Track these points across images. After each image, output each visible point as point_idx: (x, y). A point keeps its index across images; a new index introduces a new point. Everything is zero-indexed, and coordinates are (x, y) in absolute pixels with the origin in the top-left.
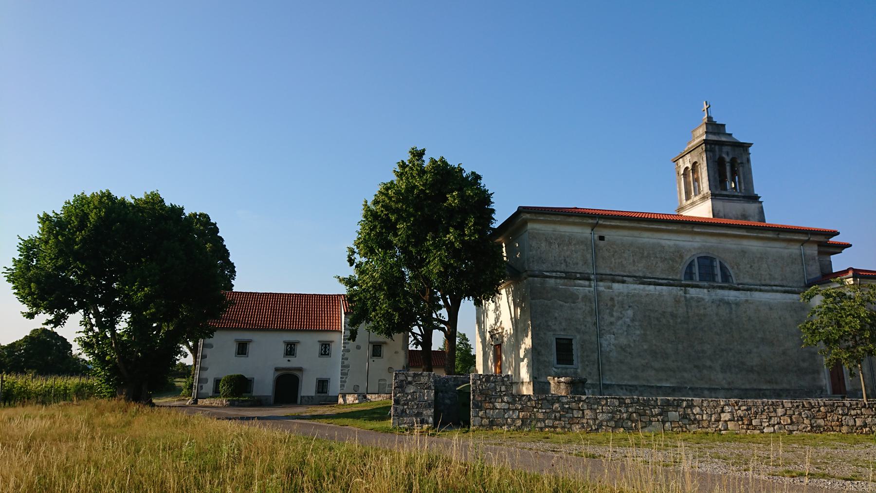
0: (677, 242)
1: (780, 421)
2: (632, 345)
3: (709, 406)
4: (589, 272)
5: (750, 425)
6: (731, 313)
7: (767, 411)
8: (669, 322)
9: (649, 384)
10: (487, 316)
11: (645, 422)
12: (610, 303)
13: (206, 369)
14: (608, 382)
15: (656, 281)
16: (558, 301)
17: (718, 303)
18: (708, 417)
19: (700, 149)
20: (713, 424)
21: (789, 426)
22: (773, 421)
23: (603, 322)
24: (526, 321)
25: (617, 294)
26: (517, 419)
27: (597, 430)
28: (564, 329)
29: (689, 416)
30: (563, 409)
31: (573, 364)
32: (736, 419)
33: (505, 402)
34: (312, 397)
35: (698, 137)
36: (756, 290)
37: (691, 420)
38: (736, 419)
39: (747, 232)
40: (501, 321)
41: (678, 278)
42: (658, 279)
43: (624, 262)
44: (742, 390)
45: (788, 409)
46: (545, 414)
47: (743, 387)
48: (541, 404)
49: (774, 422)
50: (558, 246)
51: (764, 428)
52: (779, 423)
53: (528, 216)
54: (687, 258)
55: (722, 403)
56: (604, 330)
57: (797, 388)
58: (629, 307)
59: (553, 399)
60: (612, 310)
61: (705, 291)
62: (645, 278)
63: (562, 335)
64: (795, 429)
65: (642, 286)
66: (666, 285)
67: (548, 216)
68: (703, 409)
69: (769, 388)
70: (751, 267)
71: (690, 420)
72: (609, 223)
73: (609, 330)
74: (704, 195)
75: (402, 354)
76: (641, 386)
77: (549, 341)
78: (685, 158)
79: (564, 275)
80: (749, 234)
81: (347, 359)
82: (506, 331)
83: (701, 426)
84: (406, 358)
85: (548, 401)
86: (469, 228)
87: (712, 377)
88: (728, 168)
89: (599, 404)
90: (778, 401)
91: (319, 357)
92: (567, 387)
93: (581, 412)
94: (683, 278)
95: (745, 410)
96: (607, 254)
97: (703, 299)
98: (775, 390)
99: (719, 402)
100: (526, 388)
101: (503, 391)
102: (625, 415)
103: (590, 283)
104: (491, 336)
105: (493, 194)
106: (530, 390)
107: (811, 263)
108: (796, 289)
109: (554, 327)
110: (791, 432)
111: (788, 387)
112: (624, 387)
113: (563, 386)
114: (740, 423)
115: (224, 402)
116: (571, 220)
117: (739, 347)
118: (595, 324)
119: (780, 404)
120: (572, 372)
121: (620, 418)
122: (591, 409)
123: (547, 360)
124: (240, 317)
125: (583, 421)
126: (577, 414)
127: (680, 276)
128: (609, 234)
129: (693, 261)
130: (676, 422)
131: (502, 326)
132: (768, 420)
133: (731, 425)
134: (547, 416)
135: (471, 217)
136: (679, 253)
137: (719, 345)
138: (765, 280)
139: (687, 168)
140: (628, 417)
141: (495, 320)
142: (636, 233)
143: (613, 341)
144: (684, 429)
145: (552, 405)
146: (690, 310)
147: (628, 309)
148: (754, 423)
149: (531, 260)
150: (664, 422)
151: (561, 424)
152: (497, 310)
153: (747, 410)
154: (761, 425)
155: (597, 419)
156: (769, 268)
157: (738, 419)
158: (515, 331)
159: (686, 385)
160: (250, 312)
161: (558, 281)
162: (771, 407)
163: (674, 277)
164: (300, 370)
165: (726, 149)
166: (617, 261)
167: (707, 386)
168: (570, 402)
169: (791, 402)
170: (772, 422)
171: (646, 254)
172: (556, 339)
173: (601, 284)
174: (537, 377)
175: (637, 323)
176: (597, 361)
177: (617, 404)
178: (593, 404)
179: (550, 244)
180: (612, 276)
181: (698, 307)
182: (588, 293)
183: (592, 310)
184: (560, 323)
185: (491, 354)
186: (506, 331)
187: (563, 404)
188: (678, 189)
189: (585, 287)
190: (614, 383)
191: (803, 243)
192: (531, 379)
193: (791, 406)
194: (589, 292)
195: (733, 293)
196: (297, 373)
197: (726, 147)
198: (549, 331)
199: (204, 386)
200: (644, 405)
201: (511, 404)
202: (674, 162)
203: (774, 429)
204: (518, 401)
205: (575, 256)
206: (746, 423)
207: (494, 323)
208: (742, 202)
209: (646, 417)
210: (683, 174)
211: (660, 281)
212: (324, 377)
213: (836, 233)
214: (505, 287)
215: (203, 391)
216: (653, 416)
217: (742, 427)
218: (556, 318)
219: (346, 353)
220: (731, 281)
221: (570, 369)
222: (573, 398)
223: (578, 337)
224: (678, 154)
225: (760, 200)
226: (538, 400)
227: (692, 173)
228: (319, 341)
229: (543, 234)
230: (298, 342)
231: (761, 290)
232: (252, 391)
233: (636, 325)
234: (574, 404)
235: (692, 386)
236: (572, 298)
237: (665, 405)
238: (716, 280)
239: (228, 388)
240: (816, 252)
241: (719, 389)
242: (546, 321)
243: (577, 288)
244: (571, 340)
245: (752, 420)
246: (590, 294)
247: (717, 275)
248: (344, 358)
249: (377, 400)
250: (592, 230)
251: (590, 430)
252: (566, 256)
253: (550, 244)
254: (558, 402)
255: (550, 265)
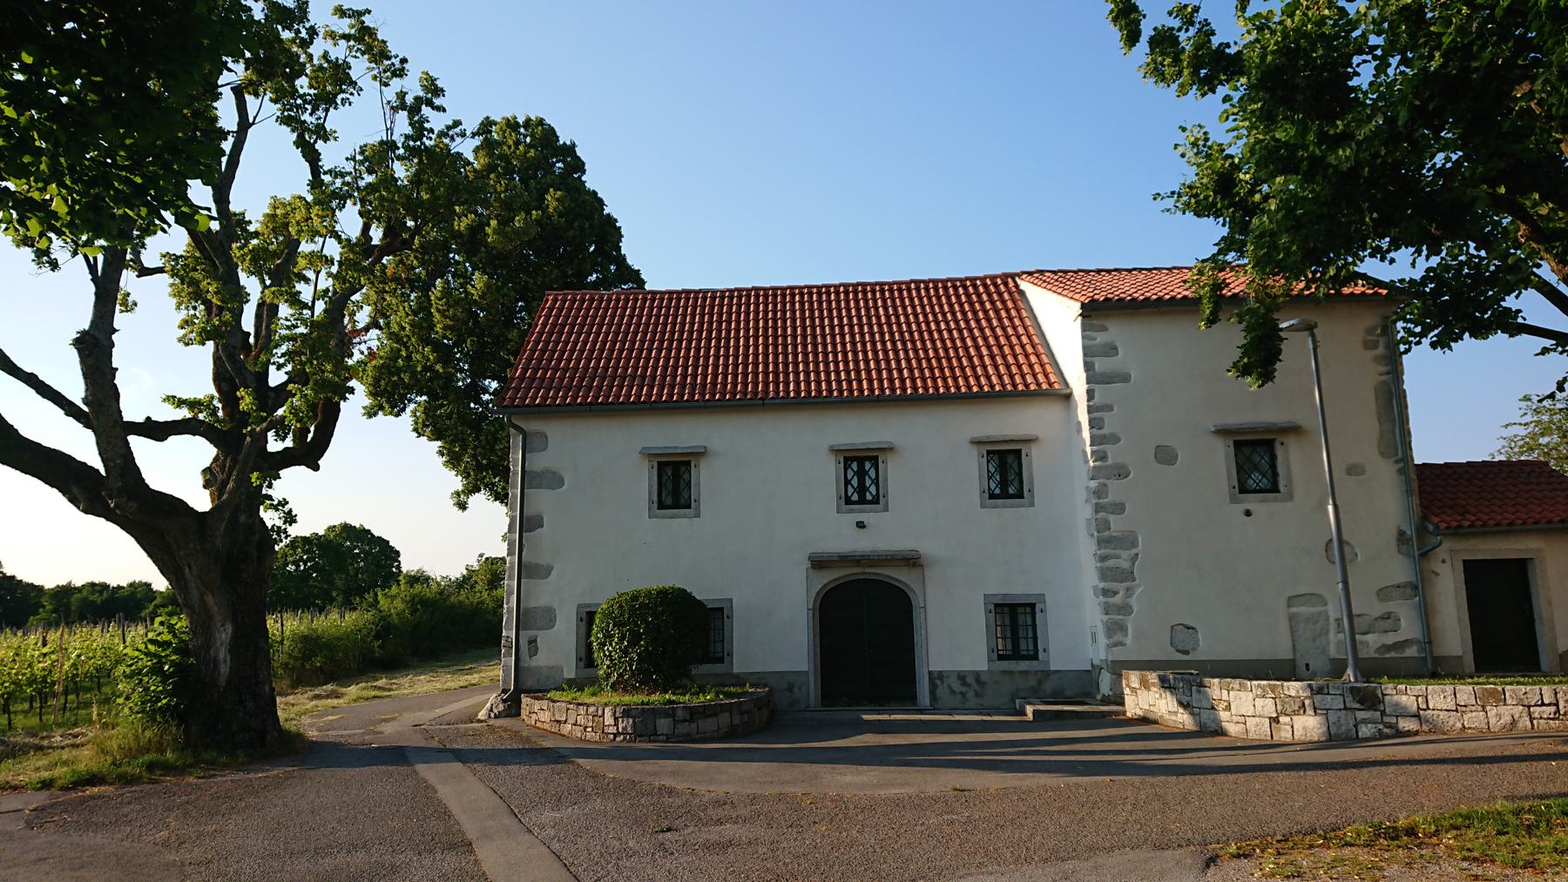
13: (543, 572)
34: (977, 675)
75: (1385, 474)
81: (1119, 508)
84: (1409, 492)
91: (983, 506)
115: (609, 720)
124: (655, 368)
160: (688, 349)
164: (912, 561)
196: (902, 576)
199: (543, 638)
212: (1018, 588)
215: (541, 660)
219: (1114, 485)
228: (977, 442)
230: (889, 449)
232: (730, 654)
239: (625, 652)
248: (1105, 508)
249: (1474, 719)
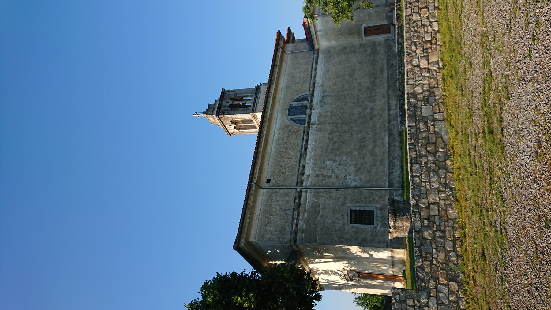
0: (277, 128)
1: (426, 17)
2: (355, 162)
3: (413, 79)
4: (295, 192)
5: (431, 42)
6: (330, 96)
7: (416, 28)
8: (337, 136)
9: (387, 152)
10: (334, 282)
11: (436, 138)
12: (321, 178)
14: (387, 183)
15: (304, 143)
16: (318, 219)
17: (322, 104)
18: (426, 79)
19: (222, 119)
20: (433, 74)
21: (430, 10)
22: (426, 23)
23: (336, 184)
24: (335, 250)
25: (314, 172)
26: (449, 288)
27: (451, 189)
28: (343, 215)
29: (425, 96)
30: (430, 227)
31: (373, 211)
32: (425, 54)
33: (428, 302)
35: (215, 120)
36: (314, 80)
37: (430, 94)
38: (425, 54)
39: (273, 85)
40: (337, 270)
41: (303, 129)
42: (303, 142)
43: (289, 165)
44: (388, 89)
45: (413, 11)
46: (438, 250)
47: (386, 88)
48: (427, 253)
49: (427, 22)
50: (272, 215)
51: (434, 30)
52: (428, 18)
53: (243, 241)
54: (289, 122)
55: (410, 67)
56: (342, 183)
57: (386, 54)
58: (324, 163)
59: (419, 239)
60: (326, 176)
61: (313, 111)
62: (301, 151)
63: (347, 218)
64: (433, 4)
65: (308, 154)
66: (308, 136)
67: (244, 223)
68: (416, 84)
69: (386, 72)
70: (298, 83)
71: (429, 96)
72: (257, 175)
73: (343, 179)
74: (252, 117)
76: (389, 158)
77: (353, 230)
78: (228, 129)
79: (296, 212)
80: (275, 83)
82: (345, 267)
83: (436, 85)
85: (422, 244)
86: (243, 301)
87: (379, 108)
88: (237, 102)
89: (419, 186)
90: (406, 20)
92: (400, 219)
93: (432, 206)
94: (303, 126)
95: (416, 47)
96: (281, 178)
97: (320, 113)
98: (388, 68)
99: (409, 70)
100: (398, 254)
101: (414, 302)
102: (431, 158)
103: (304, 192)
104: (351, 280)
105: (218, 273)
106: (399, 252)
107: (298, 48)
108: (315, 56)
109: (341, 225)
110: (436, 8)
111: (386, 60)
112: (391, 171)
113: (399, 224)
114: (429, 51)
116: (250, 204)
117: (355, 91)
118: (338, 190)
119: (408, 17)
120: (380, 212)
121: (435, 164)
122: (426, 194)
123: (370, 233)
125: (443, 204)
126: (434, 211)
127: (301, 127)
128: (266, 174)
129: (291, 119)
130: (433, 109)
131: (341, 270)
132: (425, 27)
133: (433, 59)
134: (441, 247)
135: (233, 299)
136: (285, 128)
137: (354, 103)
138: (308, 75)
139: (234, 127)
140: (433, 155)
141: (337, 275)
142: (267, 156)
143: (352, 177)
144: (441, 100)
145: (426, 239)
146: (328, 122)
147: (326, 165)
148: (430, 39)
149: (281, 240)
150: (434, 120)
151: (449, 231)
152: (327, 272)
153: (416, 45)
154: (431, 32)
155: (438, 188)
156: (300, 72)
157: (426, 53)
158: (345, 260)
159: (387, 126)
161: (301, 217)
162: (411, 25)
163: (302, 131)
165: (224, 103)
166: (287, 171)
167: (386, 112)
168: (421, 218)
169: (406, 9)
170: (427, 24)
171: (284, 150)
172: (351, 223)
173: (305, 183)
174: (386, 244)
175: (337, 158)
176: (370, 191)
177: (417, 166)
178: (420, 192)
179: (269, 222)
180: (299, 174)
181: (325, 117)
182: (312, 194)
183: (326, 191)
184: (337, 218)
185: (367, 282)
186: (345, 267)
187: (423, 226)
188: (249, 134)
189: (307, 196)
190: (388, 179)
191: (284, 52)
192: (388, 249)
193: (410, 9)
194: (311, 193)
195: (316, 94)
197: (223, 103)
198: (344, 228)
200: (417, 138)
201: (430, 293)
202: (231, 135)
203: (434, 22)
204: (425, 283)
205: (281, 203)
206: (430, 46)
207: (339, 276)
208: (259, 95)
209: (430, 138)
210: (239, 130)
211: (305, 141)
213: (279, 33)
214: (307, 264)
216: (429, 130)
217: (434, 49)
218: (333, 222)
220: (307, 95)
221: (377, 214)
222: (414, 213)
223: (349, 204)
224: (225, 133)
225: (259, 85)
226: (421, 256)
227: (238, 124)
229: (261, 228)
231: (315, 77)
233: (339, 159)
234: (422, 213)
235: (387, 122)
236: (316, 207)
237: (415, 119)
238: (306, 104)
240: (291, 45)
241: (389, 103)
242: (336, 231)
243: (307, 202)
244: (351, 211)
245: (426, 41)
246: (313, 193)
247: (302, 104)
250: (261, 188)
251: (453, 197)
252: (281, 210)
253: (269, 222)
254: (422, 232)
255: (287, 224)
